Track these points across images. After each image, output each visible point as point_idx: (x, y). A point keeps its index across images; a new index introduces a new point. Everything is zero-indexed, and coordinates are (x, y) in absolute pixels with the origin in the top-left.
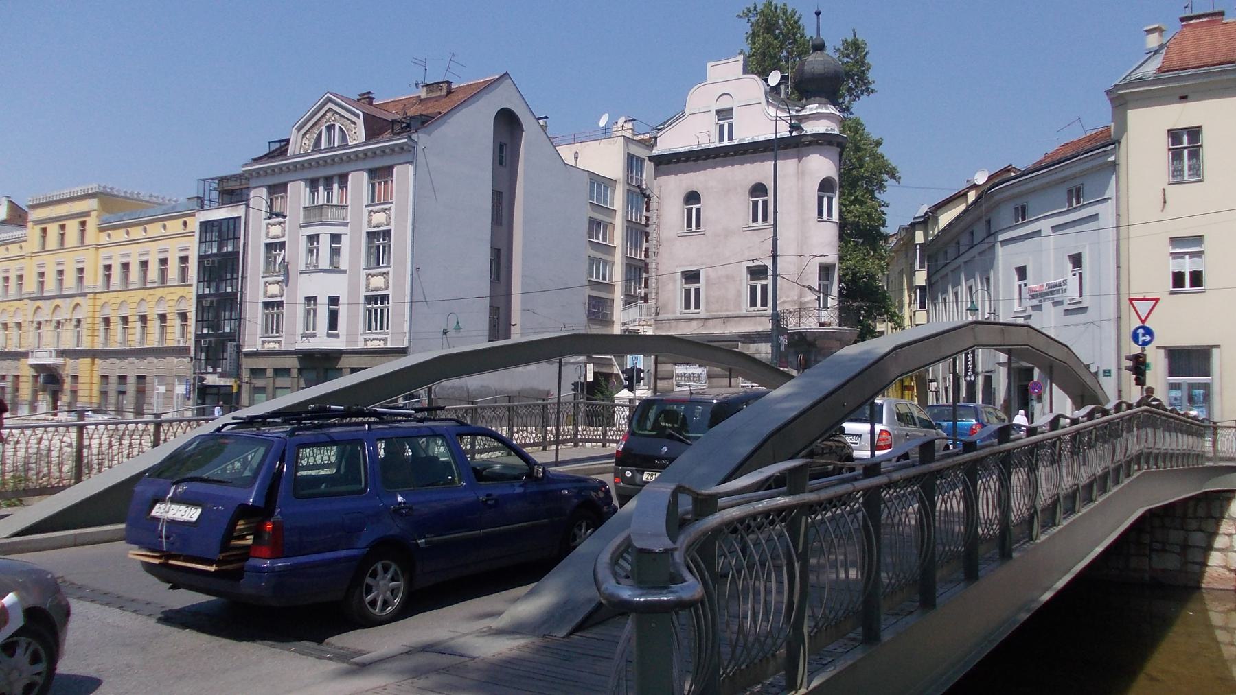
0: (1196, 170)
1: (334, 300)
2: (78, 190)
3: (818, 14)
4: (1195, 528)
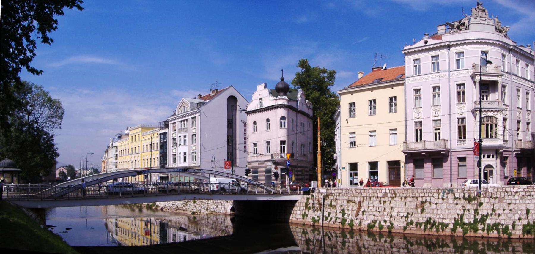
0: (375, 112)
1: (185, 154)
3: (282, 70)
4: (517, 201)
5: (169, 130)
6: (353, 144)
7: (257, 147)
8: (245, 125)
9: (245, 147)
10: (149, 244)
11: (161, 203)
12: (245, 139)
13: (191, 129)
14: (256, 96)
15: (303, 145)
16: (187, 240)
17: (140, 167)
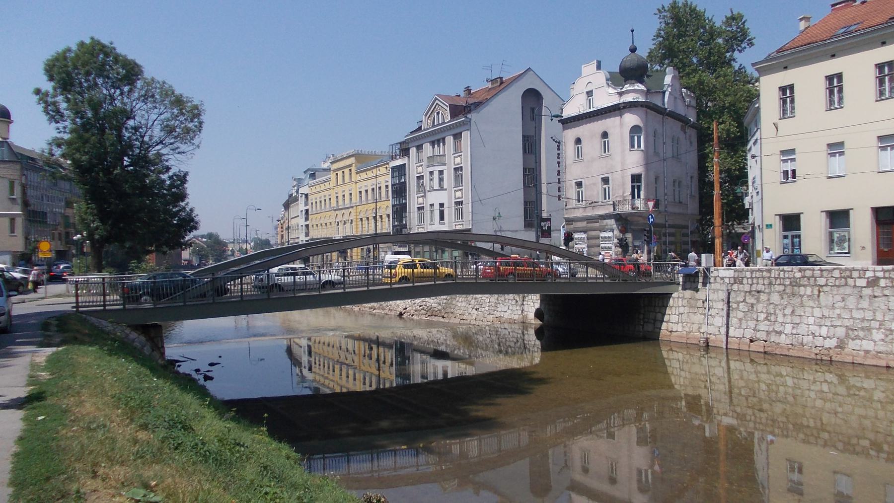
1: (442, 205)
2: (347, 153)
3: (632, 31)
5: (409, 160)
6: (790, 176)
7: (583, 189)
8: (558, 146)
9: (559, 189)
10: (374, 387)
11: (398, 302)
12: (559, 174)
13: (453, 156)
14: (580, 87)
15: (677, 183)
16: (449, 376)
17: (354, 233)
